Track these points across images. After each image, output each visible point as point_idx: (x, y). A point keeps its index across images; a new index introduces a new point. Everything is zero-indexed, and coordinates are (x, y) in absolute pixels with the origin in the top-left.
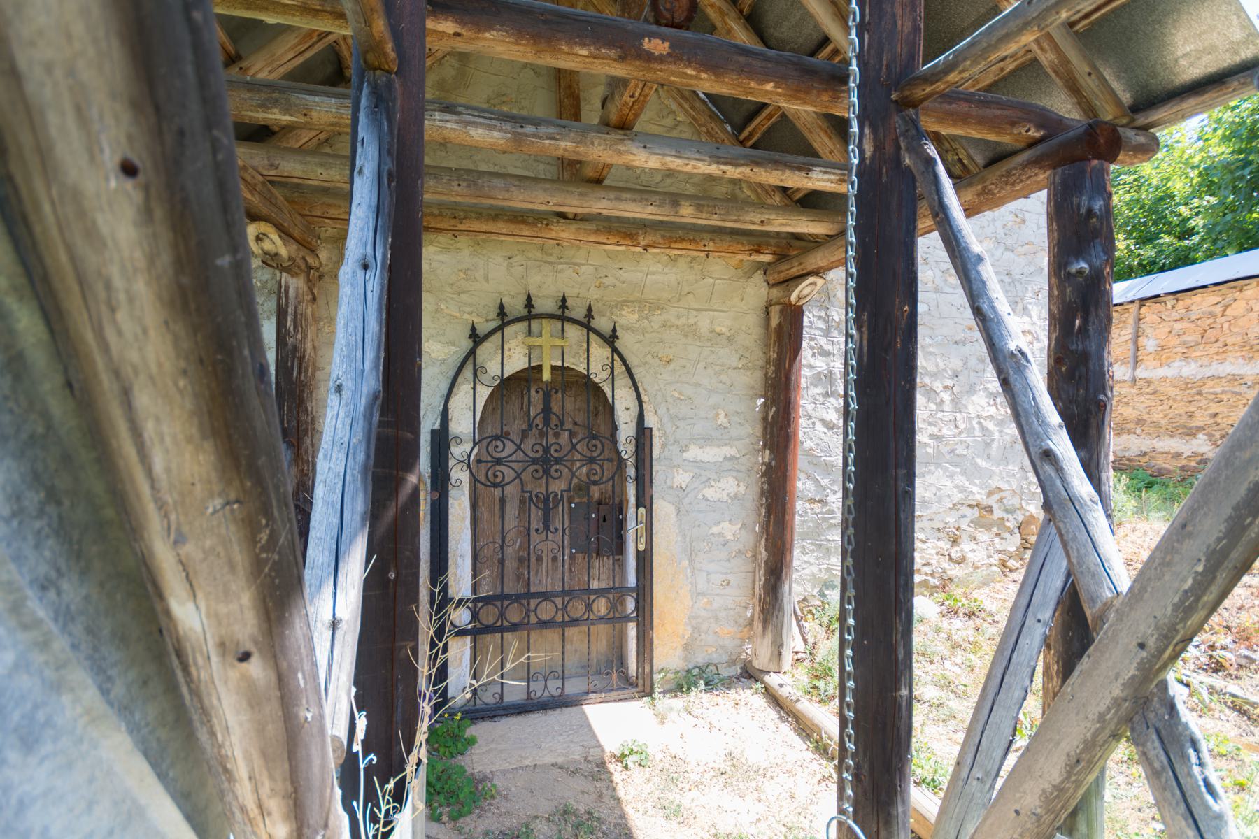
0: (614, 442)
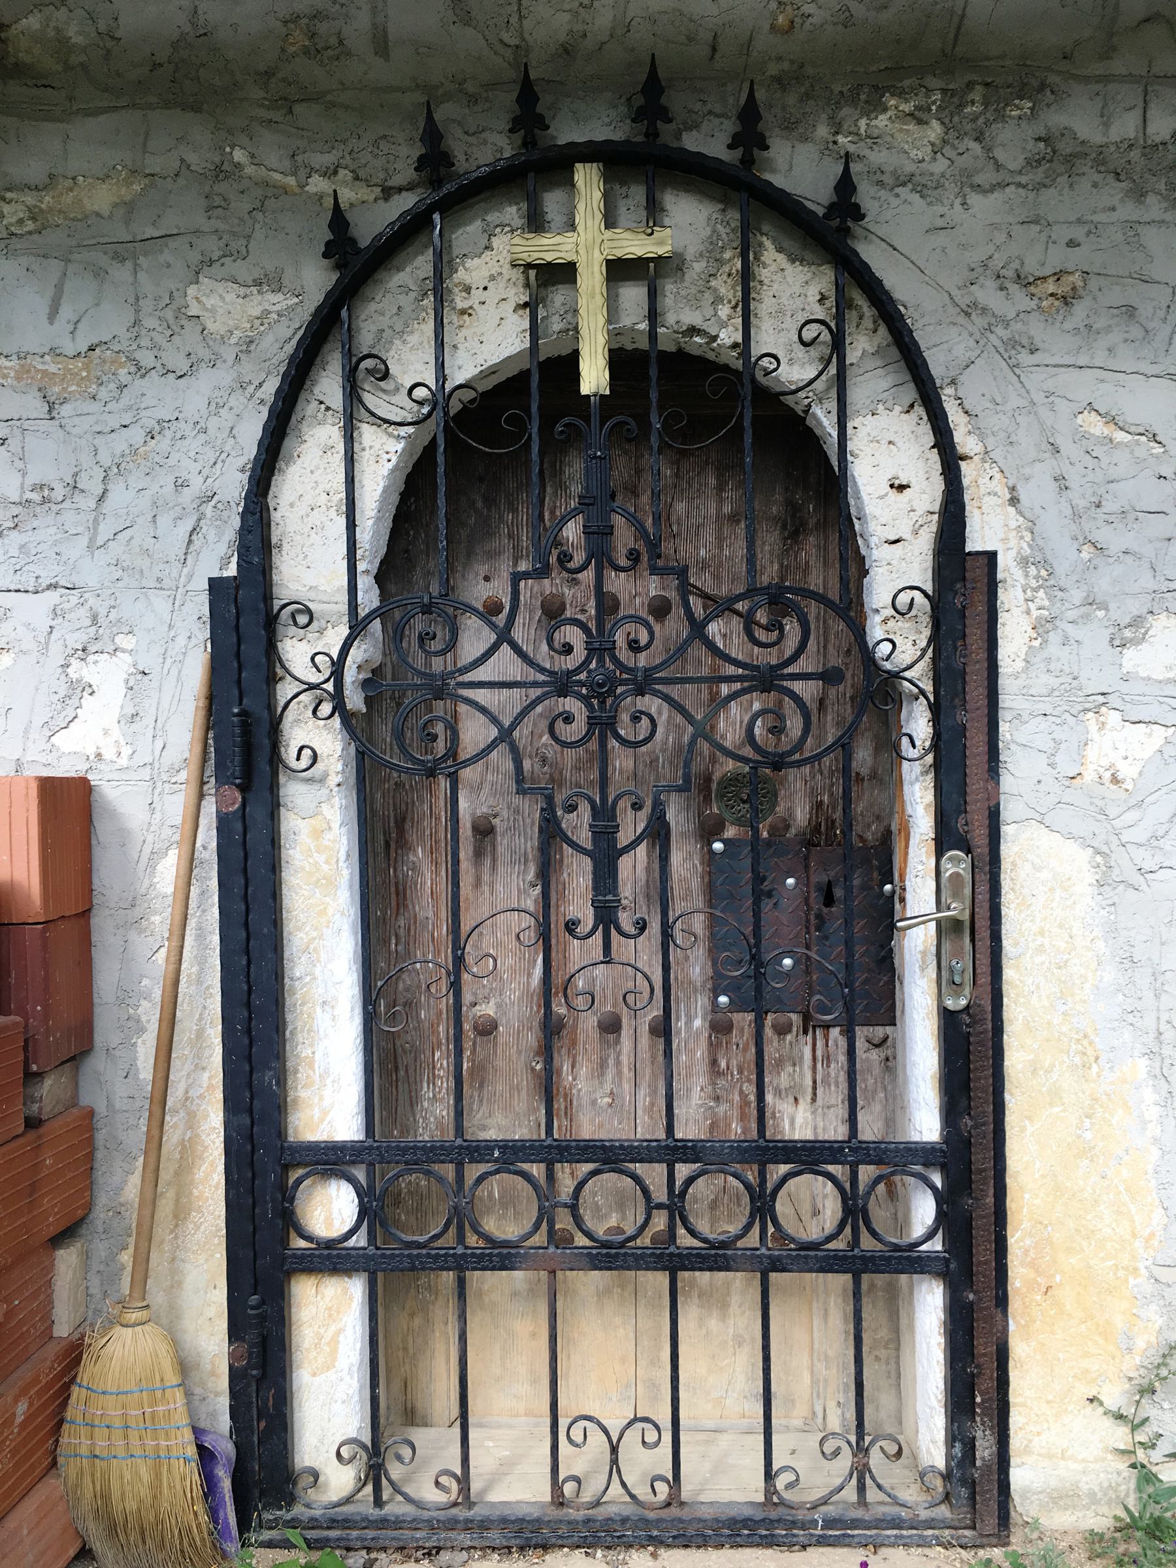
0: (850, 608)
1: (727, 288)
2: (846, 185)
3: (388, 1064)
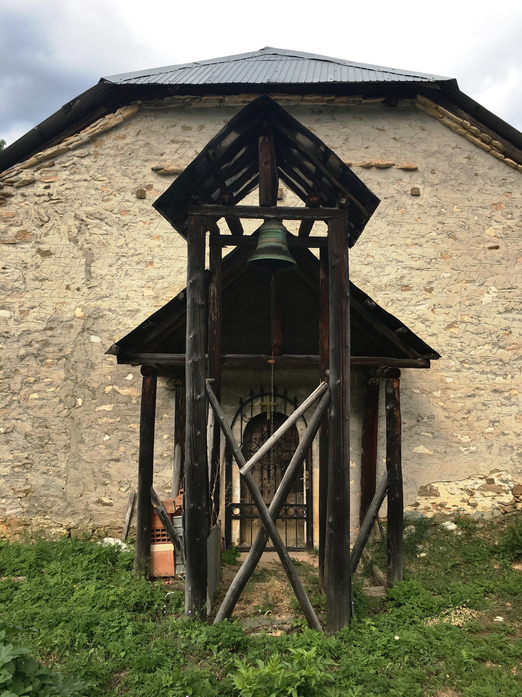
1: (283, 407)
2: (296, 398)
3: (243, 495)
